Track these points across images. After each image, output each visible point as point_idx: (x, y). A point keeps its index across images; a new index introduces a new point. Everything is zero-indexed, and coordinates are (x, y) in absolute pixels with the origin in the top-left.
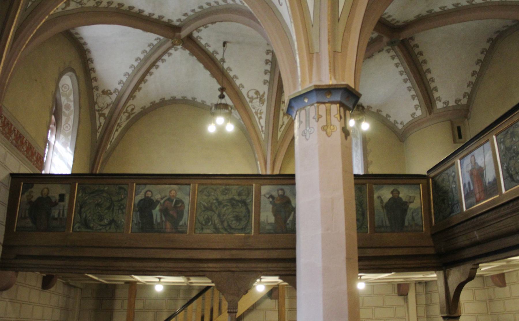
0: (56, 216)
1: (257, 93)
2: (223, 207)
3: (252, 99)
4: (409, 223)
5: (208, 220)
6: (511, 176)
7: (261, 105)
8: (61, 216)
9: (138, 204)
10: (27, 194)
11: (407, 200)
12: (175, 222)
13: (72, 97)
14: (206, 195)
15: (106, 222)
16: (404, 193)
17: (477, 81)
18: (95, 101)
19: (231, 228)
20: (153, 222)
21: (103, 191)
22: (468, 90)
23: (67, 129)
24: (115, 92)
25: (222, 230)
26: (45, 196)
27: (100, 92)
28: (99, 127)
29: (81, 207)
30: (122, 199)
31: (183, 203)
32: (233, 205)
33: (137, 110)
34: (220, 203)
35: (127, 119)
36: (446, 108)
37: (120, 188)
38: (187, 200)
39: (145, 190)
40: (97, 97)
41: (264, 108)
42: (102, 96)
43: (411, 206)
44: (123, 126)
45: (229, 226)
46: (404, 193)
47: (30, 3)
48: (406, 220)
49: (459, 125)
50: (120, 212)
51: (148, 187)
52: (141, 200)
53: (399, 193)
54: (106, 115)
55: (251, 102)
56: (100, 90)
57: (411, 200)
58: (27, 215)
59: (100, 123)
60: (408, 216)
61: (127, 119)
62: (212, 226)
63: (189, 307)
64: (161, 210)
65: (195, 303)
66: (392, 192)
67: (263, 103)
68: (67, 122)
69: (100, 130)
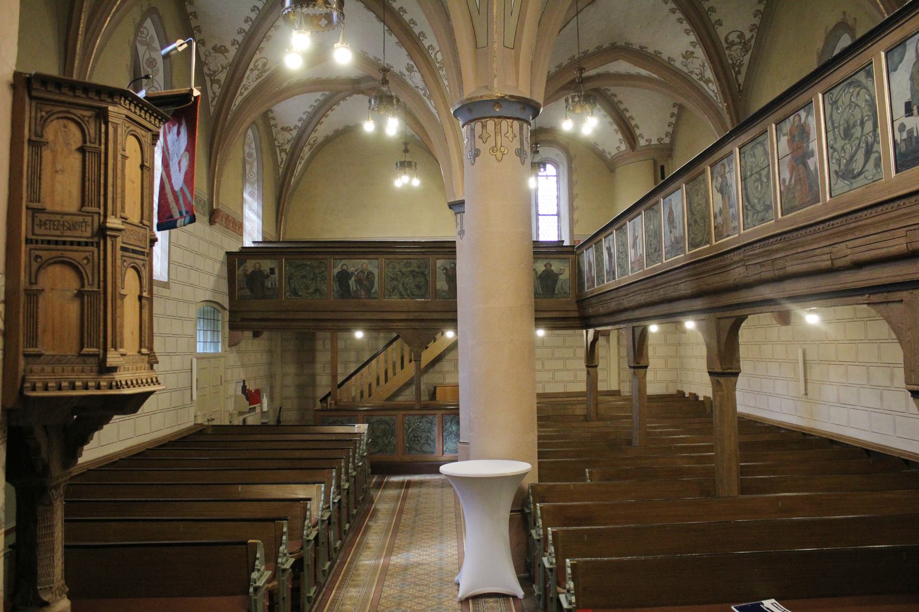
0: (270, 286)
2: (406, 278)
4: (559, 291)
5: (394, 288)
6: (620, 265)
8: (274, 286)
9: (337, 275)
10: (241, 268)
11: (558, 273)
12: (368, 291)
13: (253, 146)
14: (391, 268)
15: (311, 290)
16: (556, 266)
17: (677, 120)
18: (274, 137)
19: (413, 295)
20: (350, 291)
21: (306, 265)
22: (670, 130)
23: (251, 177)
24: (295, 128)
25: (406, 296)
26: (257, 270)
28: (282, 163)
29: (290, 279)
30: (323, 272)
31: (373, 274)
32: (414, 276)
33: (320, 140)
34: (403, 274)
35: (309, 151)
36: (649, 147)
37: (320, 262)
38: (376, 272)
39: (341, 264)
43: (561, 277)
45: (412, 293)
46: (556, 266)
47: (370, 440)
48: (556, 289)
49: (662, 163)
50: (322, 282)
51: (344, 262)
52: (339, 272)
53: (551, 266)
54: (288, 151)
56: (279, 128)
57: (562, 272)
58: (245, 286)
59: (282, 159)
60: (558, 286)
62: (398, 293)
63: (390, 349)
64: (355, 281)
65: (395, 343)
66: (545, 266)
68: (251, 168)
69: (282, 166)
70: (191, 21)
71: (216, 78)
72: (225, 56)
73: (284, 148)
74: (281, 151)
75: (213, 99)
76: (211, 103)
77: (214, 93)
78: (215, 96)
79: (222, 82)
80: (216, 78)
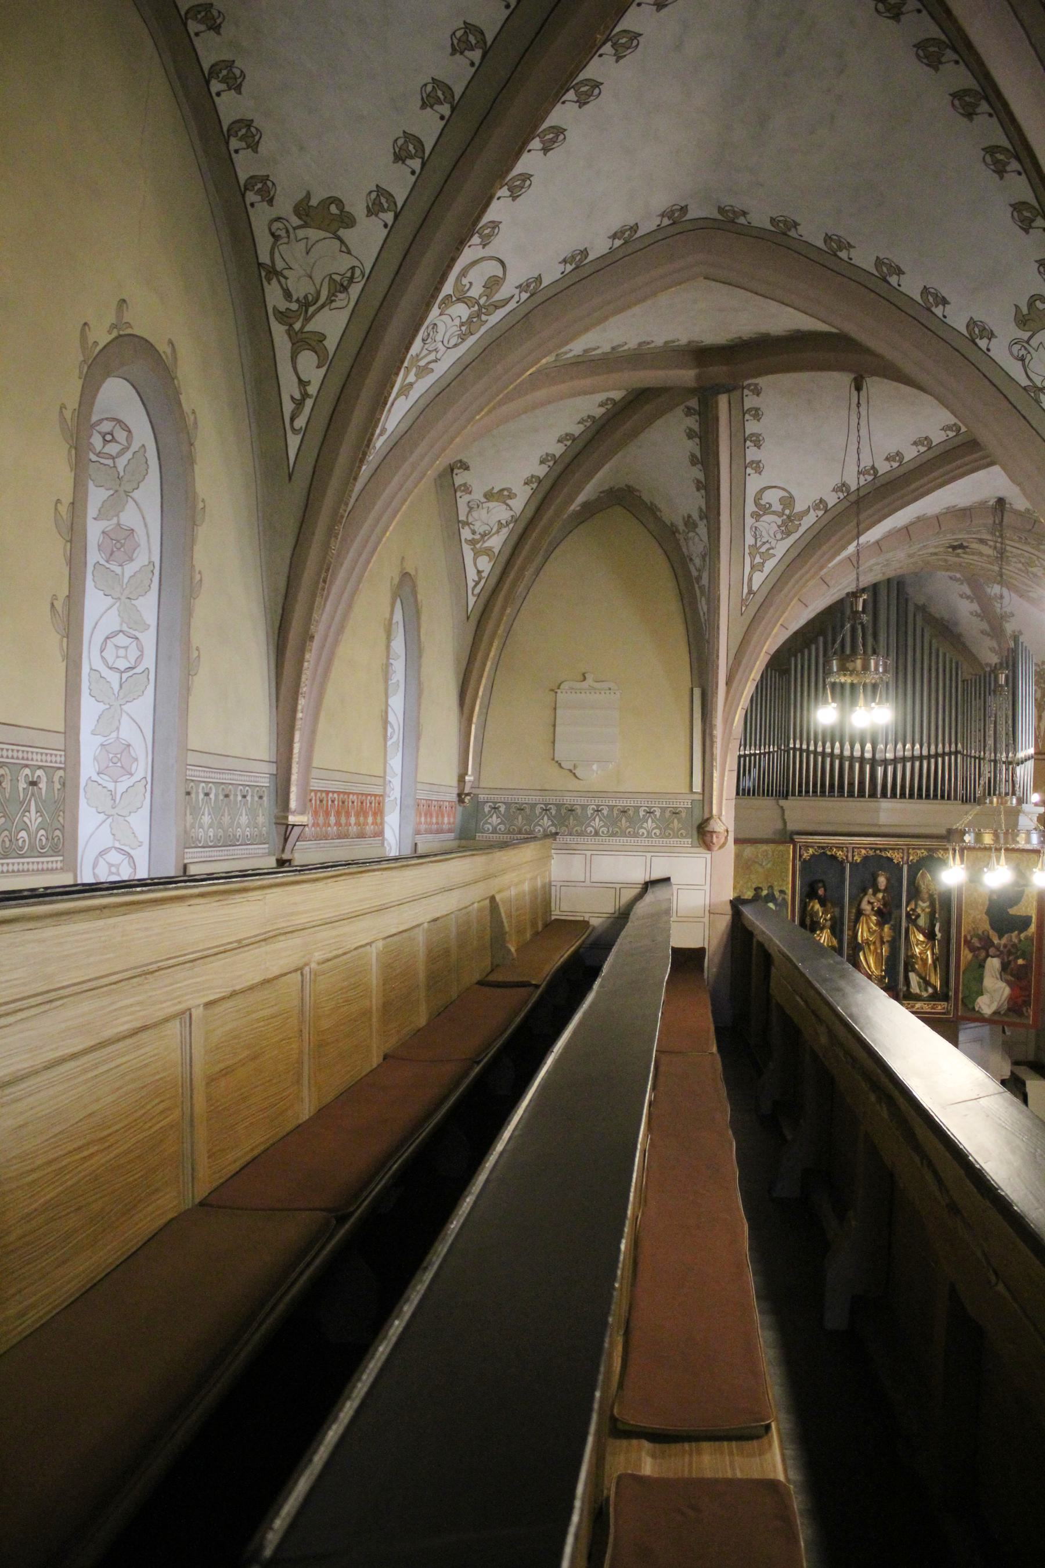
1: (788, 501)
3: (763, 510)
7: (779, 536)
27: (284, 206)
40: (471, 509)
41: (781, 548)
42: (301, 233)
44: (440, 369)
55: (757, 516)
56: (284, 206)
61: (463, 338)
67: (788, 534)
70: (198, 43)
71: (309, 328)
72: (507, 505)
73: (486, 545)
74: (300, 342)
75: (299, 404)
76: (292, 420)
77: (303, 383)
78: (305, 395)
79: (331, 344)
80: (309, 328)
